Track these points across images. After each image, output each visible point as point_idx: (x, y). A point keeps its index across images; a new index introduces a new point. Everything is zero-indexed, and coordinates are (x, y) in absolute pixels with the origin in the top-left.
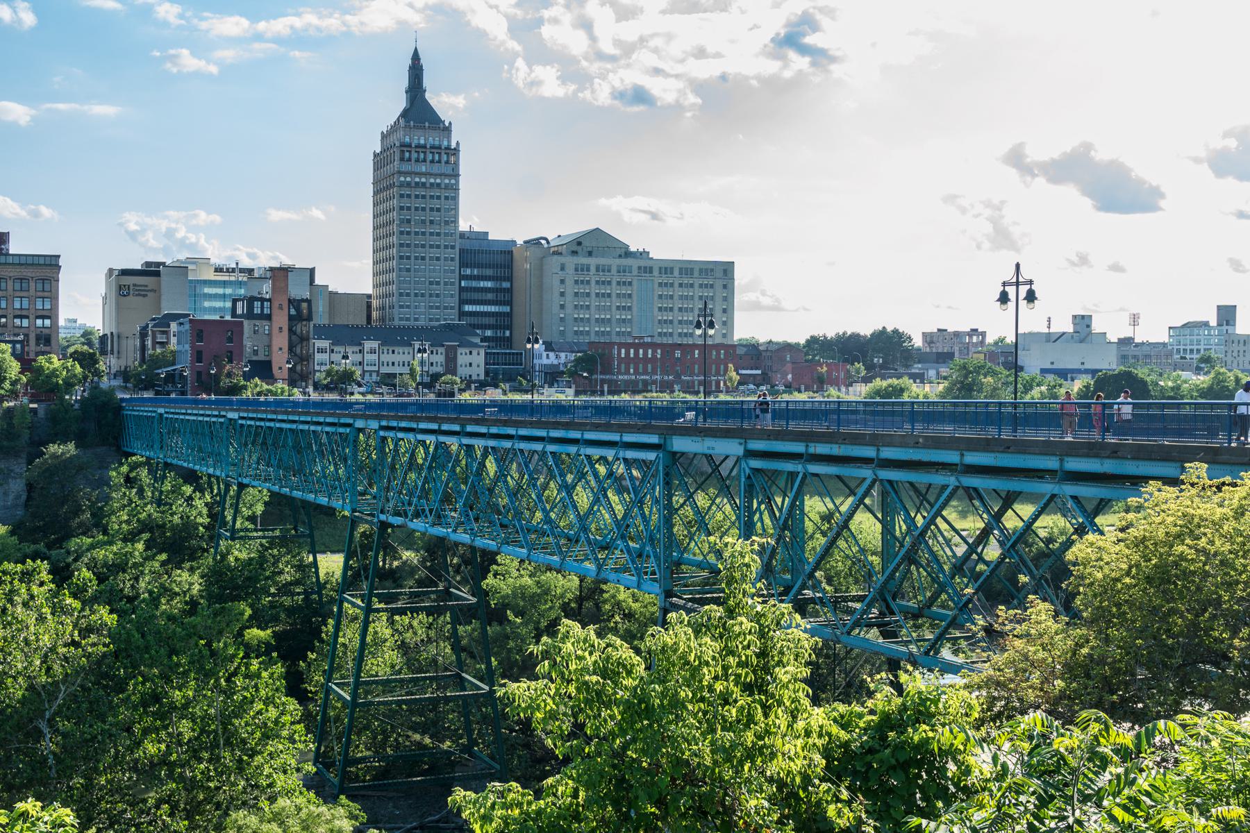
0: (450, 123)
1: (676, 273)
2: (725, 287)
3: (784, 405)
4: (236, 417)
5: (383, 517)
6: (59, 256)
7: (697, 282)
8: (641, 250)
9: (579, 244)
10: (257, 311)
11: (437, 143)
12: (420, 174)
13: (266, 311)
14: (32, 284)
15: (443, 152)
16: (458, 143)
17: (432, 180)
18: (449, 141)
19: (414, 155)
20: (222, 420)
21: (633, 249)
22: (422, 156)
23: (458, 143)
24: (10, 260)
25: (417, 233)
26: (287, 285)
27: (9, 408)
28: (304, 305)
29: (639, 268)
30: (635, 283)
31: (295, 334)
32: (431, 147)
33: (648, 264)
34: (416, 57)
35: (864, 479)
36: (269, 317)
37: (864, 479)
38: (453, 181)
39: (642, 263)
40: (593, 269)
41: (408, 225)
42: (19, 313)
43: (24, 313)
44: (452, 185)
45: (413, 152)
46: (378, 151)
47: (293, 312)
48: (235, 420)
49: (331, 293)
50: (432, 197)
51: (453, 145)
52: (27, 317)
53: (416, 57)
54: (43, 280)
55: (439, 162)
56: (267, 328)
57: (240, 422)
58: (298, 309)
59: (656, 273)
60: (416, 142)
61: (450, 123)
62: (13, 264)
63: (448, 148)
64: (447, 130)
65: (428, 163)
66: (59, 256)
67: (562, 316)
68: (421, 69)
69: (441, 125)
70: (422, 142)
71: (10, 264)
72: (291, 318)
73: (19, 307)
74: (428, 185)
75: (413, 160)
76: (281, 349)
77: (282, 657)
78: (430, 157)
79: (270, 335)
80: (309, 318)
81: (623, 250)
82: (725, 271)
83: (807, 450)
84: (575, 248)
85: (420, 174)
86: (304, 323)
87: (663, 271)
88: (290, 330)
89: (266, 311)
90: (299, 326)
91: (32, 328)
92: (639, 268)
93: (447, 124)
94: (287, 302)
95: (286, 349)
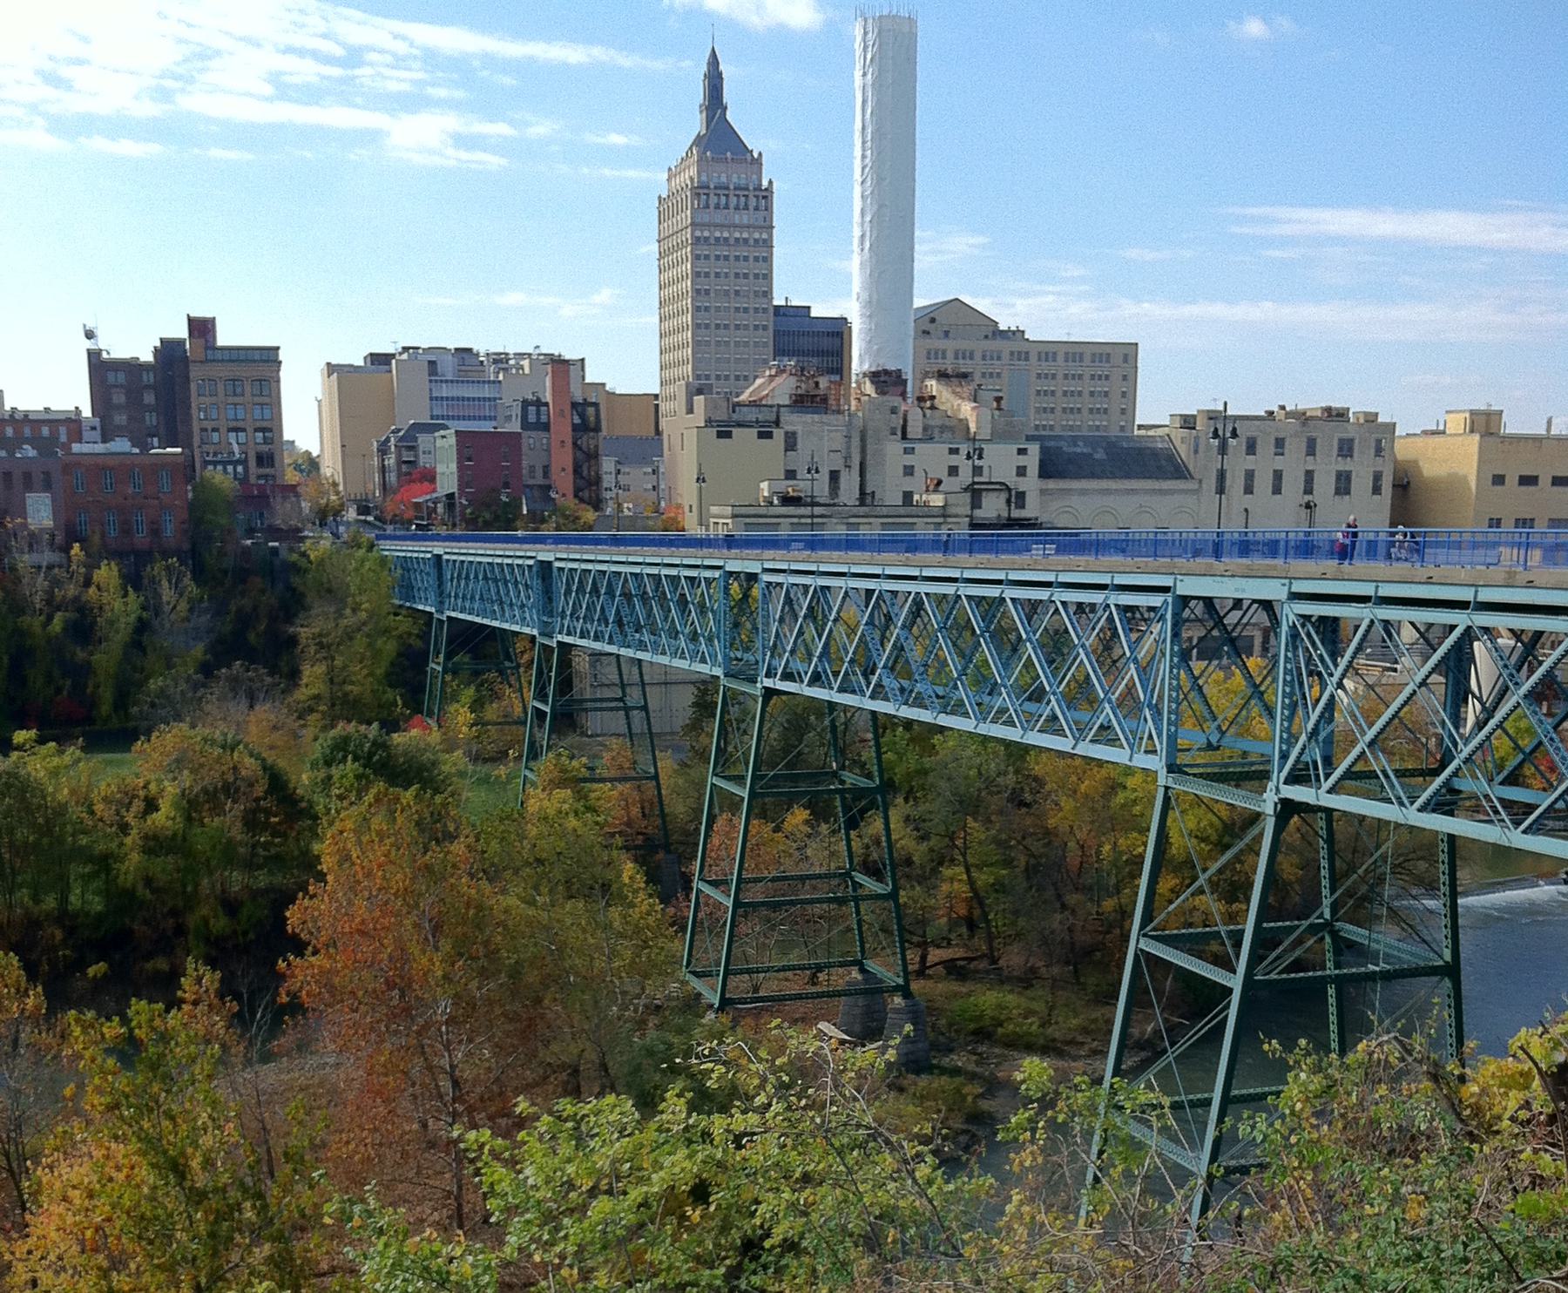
0: (760, 154)
1: (1060, 358)
2: (1125, 378)
3: (1094, 537)
4: (552, 559)
5: (768, 683)
6: (278, 348)
7: (1087, 373)
8: (1013, 328)
9: (933, 320)
10: (532, 418)
11: (743, 182)
12: (741, 227)
13: (544, 419)
14: (220, 387)
15: (751, 195)
16: (771, 182)
17: (737, 235)
18: (760, 180)
19: (713, 200)
20: (531, 562)
21: (1002, 327)
22: (723, 199)
23: (771, 182)
24: (219, 355)
25: (718, 309)
26: (568, 384)
27: (273, 547)
28: (591, 410)
29: (1012, 353)
30: (1005, 375)
31: (580, 449)
32: (716, 188)
33: (1024, 347)
34: (714, 61)
35: (1453, 628)
36: (546, 427)
37: (1453, 628)
38: (765, 236)
39: (1016, 346)
40: (978, 355)
41: (706, 298)
42: (258, 424)
43: (241, 424)
44: (765, 241)
45: (712, 195)
46: (664, 195)
47: (577, 420)
48: (550, 563)
49: (608, 393)
50: (737, 258)
51: (765, 183)
52: (243, 430)
53: (714, 61)
54: (234, 380)
55: (727, 207)
56: (545, 441)
57: (557, 564)
58: (582, 416)
59: (1033, 359)
60: (716, 180)
61: (760, 154)
62: (223, 360)
63: (758, 188)
64: (757, 162)
65: (732, 210)
66: (278, 348)
67: (1122, 423)
68: (720, 75)
69: (749, 158)
70: (724, 179)
71: (219, 361)
72: (575, 428)
73: (232, 417)
74: (732, 241)
75: (712, 206)
76: (563, 470)
77: (130, 893)
78: (733, 200)
79: (548, 451)
80: (597, 429)
81: (991, 329)
82: (1126, 359)
83: (1376, 592)
84: (928, 327)
85: (741, 227)
86: (592, 434)
87: (1043, 356)
88: (575, 444)
89: (544, 419)
90: (585, 438)
91: (251, 444)
92: (1012, 353)
93: (756, 155)
94: (569, 407)
95: (570, 469)
